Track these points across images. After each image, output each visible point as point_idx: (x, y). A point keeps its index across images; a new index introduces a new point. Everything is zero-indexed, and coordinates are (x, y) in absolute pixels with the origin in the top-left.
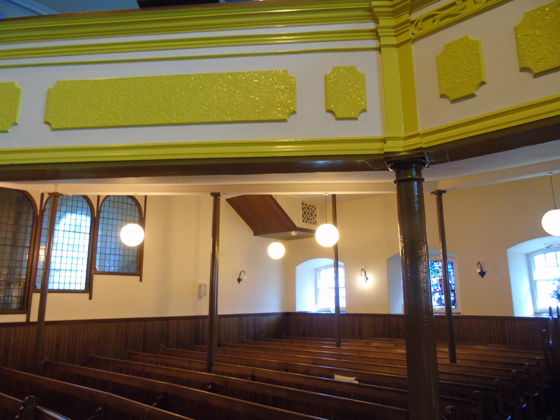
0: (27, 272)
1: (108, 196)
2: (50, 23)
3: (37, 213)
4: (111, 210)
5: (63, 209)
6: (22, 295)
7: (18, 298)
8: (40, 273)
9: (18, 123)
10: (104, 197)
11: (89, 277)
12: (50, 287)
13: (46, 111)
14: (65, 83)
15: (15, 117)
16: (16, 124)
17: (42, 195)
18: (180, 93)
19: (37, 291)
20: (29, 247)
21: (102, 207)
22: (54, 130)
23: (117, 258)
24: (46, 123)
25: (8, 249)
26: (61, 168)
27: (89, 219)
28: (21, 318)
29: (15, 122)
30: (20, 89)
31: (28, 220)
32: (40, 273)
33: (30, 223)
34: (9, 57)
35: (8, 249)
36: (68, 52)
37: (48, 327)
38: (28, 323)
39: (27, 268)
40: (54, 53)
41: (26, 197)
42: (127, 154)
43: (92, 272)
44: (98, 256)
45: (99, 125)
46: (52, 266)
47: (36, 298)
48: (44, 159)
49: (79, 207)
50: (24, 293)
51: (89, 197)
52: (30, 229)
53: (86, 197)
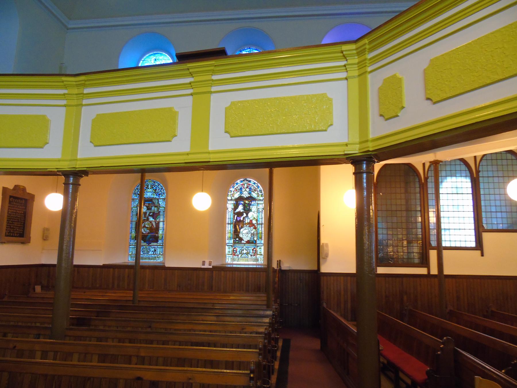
0: (422, 232)
1: (484, 155)
2: (416, 11)
3: (422, 181)
4: (490, 168)
5: (443, 173)
6: (421, 251)
7: (162, 249)
8: (434, 232)
9: (404, 106)
10: (481, 157)
11: (477, 234)
12: (444, 244)
13: (426, 89)
14: (437, 58)
15: (401, 102)
16: (403, 108)
17: (424, 164)
18: (502, 47)
19: (433, 248)
20: (420, 211)
21: (481, 167)
22: (435, 103)
23: (504, 215)
24: (428, 99)
25: (161, 233)
26: (436, 138)
27: (468, 180)
28: (423, 271)
29: (402, 106)
30: (401, 78)
31: (415, 188)
32: (434, 232)
33: (418, 190)
34: (447, 26)
35: (161, 233)
36: (456, 19)
37: (447, 280)
38: (429, 276)
39: (422, 229)
40: (455, 19)
41: (410, 167)
42: (496, 110)
43: (481, 230)
44: (484, 215)
45: (477, 86)
46: (443, 226)
47: (433, 254)
48: (425, 132)
49: (497, 164)
50: (423, 250)
51: (465, 159)
52: (418, 195)
53: (462, 160)
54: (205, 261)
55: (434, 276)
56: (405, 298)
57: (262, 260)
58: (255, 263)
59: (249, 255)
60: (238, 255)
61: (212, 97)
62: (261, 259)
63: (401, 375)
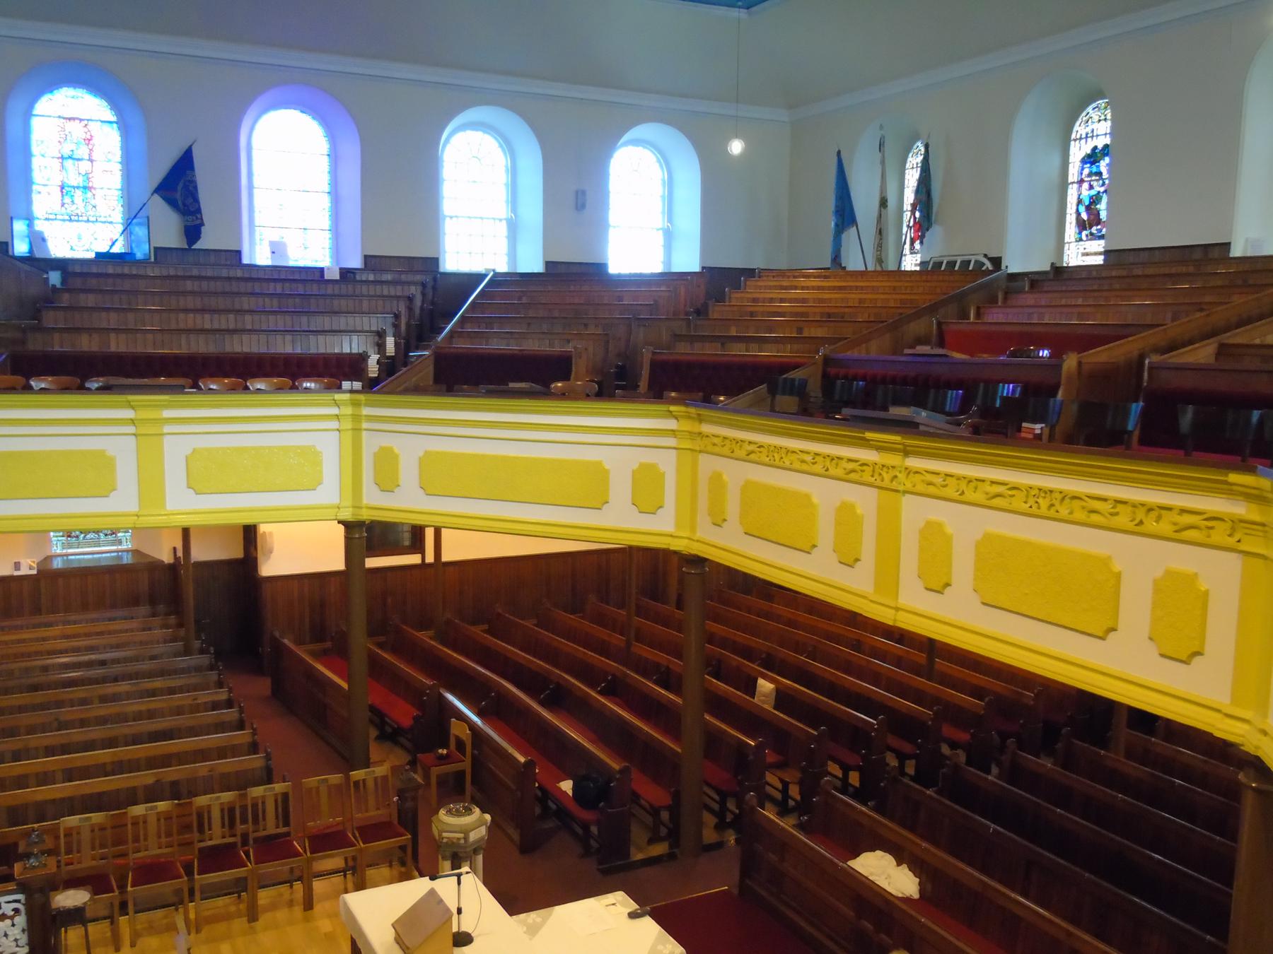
16: (399, 486)
28: (414, 559)
38: (424, 565)
54: (19, 563)
55: (430, 565)
56: (389, 600)
57: (128, 541)
58: (114, 548)
59: (101, 534)
60: (77, 537)
61: (165, 440)
62: (126, 539)
63: (387, 719)
